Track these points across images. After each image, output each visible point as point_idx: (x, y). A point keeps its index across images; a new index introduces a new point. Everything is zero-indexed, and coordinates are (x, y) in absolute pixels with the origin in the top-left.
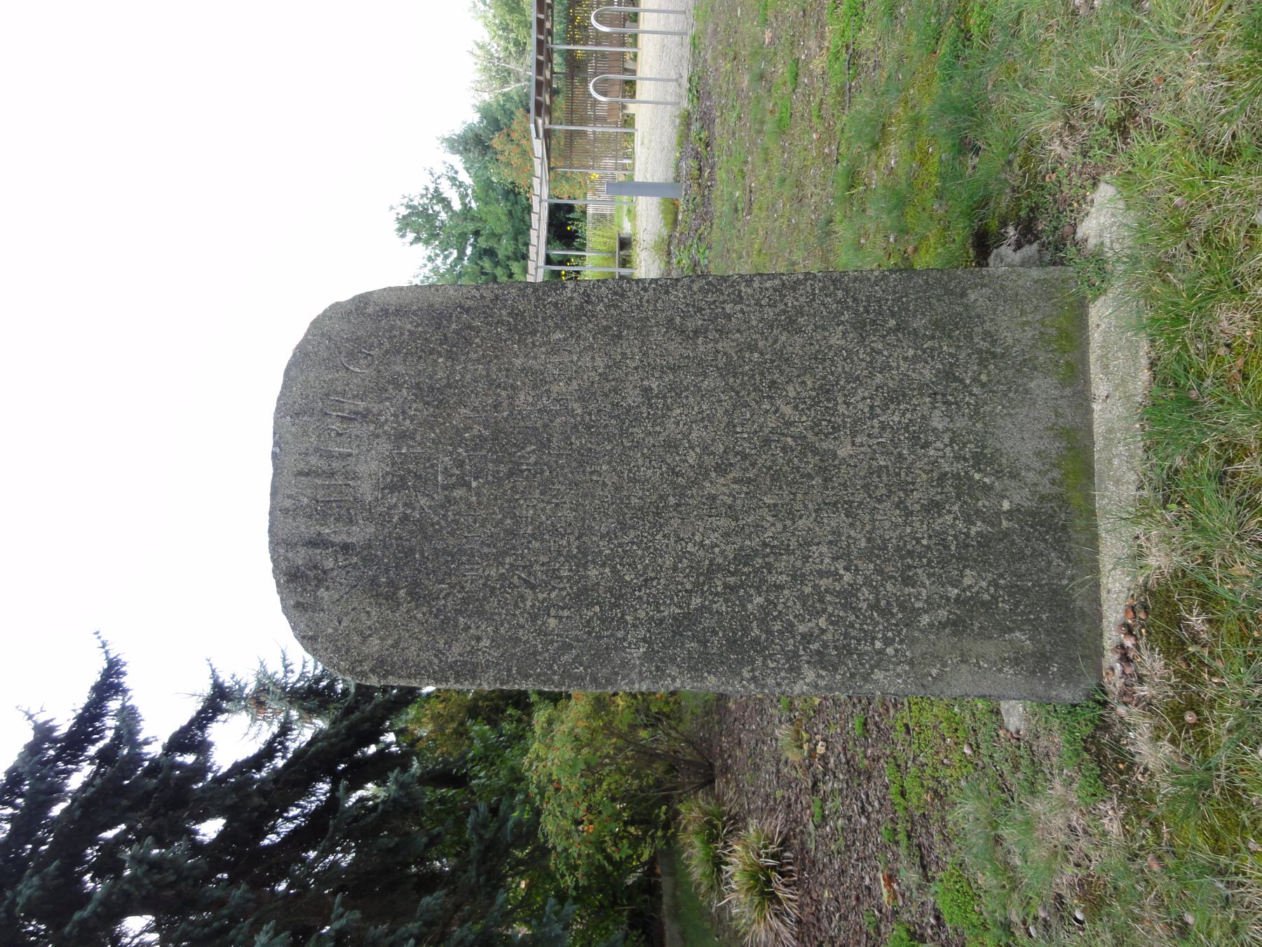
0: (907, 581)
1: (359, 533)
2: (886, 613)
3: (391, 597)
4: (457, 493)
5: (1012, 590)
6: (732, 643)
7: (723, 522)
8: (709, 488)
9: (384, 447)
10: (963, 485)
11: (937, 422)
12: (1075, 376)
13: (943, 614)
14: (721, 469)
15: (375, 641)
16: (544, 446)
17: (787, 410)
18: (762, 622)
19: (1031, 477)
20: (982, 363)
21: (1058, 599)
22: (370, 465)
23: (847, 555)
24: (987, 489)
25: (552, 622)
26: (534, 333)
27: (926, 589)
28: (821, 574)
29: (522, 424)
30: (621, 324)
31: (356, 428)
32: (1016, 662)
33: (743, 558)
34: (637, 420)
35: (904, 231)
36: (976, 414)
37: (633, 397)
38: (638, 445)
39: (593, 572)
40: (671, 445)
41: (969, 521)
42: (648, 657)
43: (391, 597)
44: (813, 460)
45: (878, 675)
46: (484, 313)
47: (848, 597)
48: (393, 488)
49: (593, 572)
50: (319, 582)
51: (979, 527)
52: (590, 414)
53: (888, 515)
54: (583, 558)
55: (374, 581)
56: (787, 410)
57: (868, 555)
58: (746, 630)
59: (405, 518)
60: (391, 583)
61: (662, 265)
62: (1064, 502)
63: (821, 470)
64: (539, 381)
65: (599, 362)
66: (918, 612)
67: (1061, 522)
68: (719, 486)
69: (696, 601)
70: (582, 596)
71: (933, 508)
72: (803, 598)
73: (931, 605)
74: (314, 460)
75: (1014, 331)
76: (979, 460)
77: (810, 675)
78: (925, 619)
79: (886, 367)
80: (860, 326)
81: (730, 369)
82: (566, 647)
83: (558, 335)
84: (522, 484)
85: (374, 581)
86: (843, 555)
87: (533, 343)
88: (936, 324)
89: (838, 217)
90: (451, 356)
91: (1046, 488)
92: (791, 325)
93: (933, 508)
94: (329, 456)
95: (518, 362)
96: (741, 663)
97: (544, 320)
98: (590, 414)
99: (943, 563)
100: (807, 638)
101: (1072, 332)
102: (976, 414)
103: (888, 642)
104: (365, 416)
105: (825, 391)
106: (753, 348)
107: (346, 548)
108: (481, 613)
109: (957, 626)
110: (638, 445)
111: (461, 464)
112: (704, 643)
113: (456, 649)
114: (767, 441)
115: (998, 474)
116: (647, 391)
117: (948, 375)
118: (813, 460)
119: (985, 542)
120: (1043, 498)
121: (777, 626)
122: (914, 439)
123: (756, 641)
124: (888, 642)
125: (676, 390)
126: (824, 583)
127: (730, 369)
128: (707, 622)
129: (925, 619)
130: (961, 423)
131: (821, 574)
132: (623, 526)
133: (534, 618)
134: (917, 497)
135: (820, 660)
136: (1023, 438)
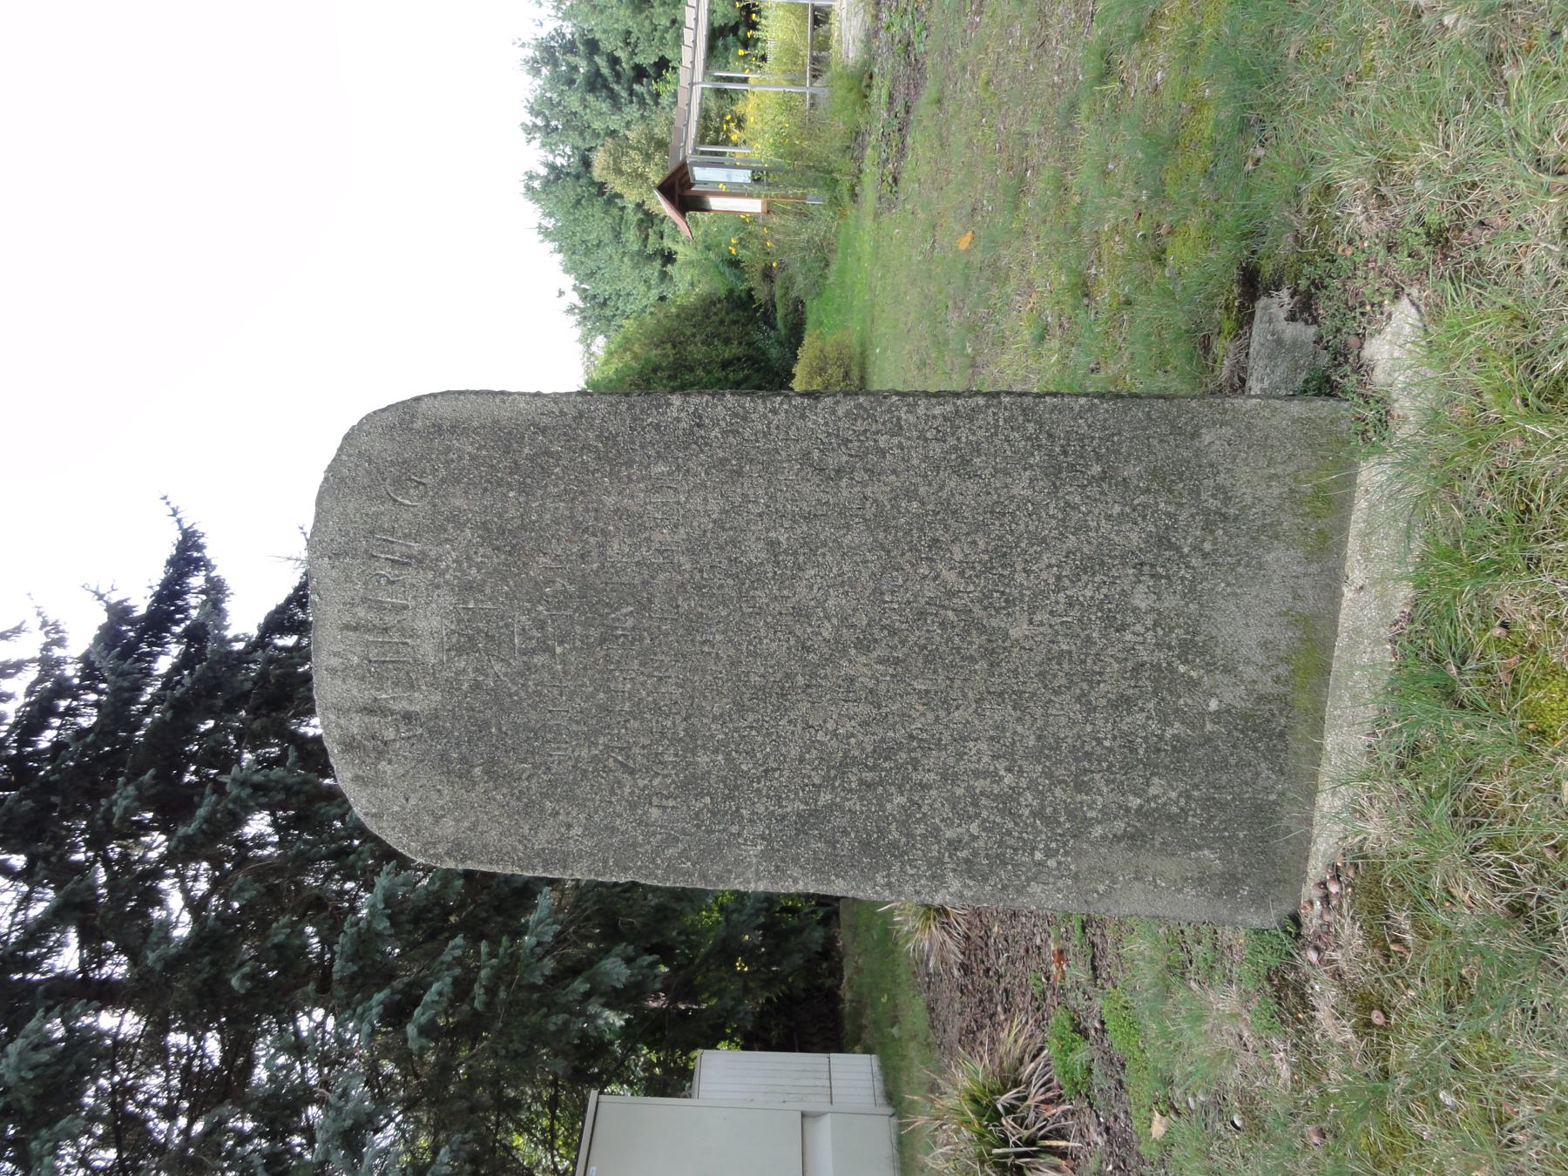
0: (1080, 787)
1: (423, 701)
2: (1051, 821)
3: (465, 774)
4: (539, 660)
5: (1208, 803)
6: (865, 845)
7: (863, 709)
8: (846, 668)
9: (447, 599)
10: (1164, 679)
11: (1141, 600)
12: (1325, 549)
13: (1120, 826)
14: (864, 646)
15: (449, 822)
16: (643, 607)
17: (950, 577)
18: (903, 825)
19: (1250, 672)
20: (1208, 527)
21: (1262, 816)
22: (431, 623)
23: (1010, 755)
24: (1193, 684)
25: (655, 813)
26: (629, 464)
27: (1103, 796)
28: (977, 774)
29: (615, 579)
30: (742, 456)
31: (410, 575)
32: (1201, 882)
33: (885, 751)
34: (760, 581)
35: (1158, 194)
36: (1191, 592)
37: (755, 552)
38: (760, 612)
39: (703, 759)
40: (802, 614)
41: (1165, 721)
42: (765, 856)
43: (465, 774)
44: (978, 640)
45: (1035, 888)
46: (565, 434)
47: (1007, 802)
48: (460, 650)
49: (703, 759)
50: (380, 755)
51: (1177, 728)
52: (701, 571)
53: (1066, 708)
54: (691, 741)
55: (444, 757)
56: (950, 577)
57: (1036, 756)
58: (882, 833)
59: (477, 686)
60: (463, 759)
61: (869, 19)
62: (1286, 703)
63: (988, 653)
64: (636, 526)
65: (714, 506)
66: (1090, 823)
67: (1277, 731)
68: (860, 667)
69: (825, 798)
70: (691, 784)
71: (1123, 703)
72: (954, 802)
73: (1106, 815)
74: (361, 612)
75: (1254, 485)
76: (1187, 649)
77: (956, 885)
78: (1098, 831)
79: (1082, 528)
80: (1053, 471)
81: (881, 521)
82: (672, 840)
83: (661, 468)
84: (617, 653)
85: (444, 757)
86: (1008, 755)
87: (629, 477)
88: (1154, 473)
89: (1084, 108)
90: (524, 489)
91: (1267, 686)
92: (963, 467)
93: (1123, 703)
94: (380, 607)
95: (610, 501)
96: (875, 868)
97: (642, 447)
98: (701, 571)
99: (1127, 768)
100: (955, 845)
101: (1331, 504)
102: (1191, 592)
103: (1050, 853)
104: (420, 561)
105: (1001, 554)
106: (911, 494)
107: (408, 717)
108: (570, 798)
109: (1134, 839)
110: (760, 612)
111: (542, 626)
112: (833, 844)
113: (543, 836)
114: (922, 614)
115: (1210, 667)
116: (773, 544)
117: (1162, 541)
118: (978, 640)
119: (1181, 747)
120: (1261, 698)
121: (920, 830)
122: (1109, 619)
123: (894, 845)
124: (1050, 853)
125: (810, 545)
126: (980, 784)
127: (881, 521)
128: (838, 821)
129: (1098, 831)
130: (1171, 602)
131: (977, 774)
132: (741, 709)
133: (633, 806)
134: (1106, 689)
135: (969, 868)
136: (1246, 625)
